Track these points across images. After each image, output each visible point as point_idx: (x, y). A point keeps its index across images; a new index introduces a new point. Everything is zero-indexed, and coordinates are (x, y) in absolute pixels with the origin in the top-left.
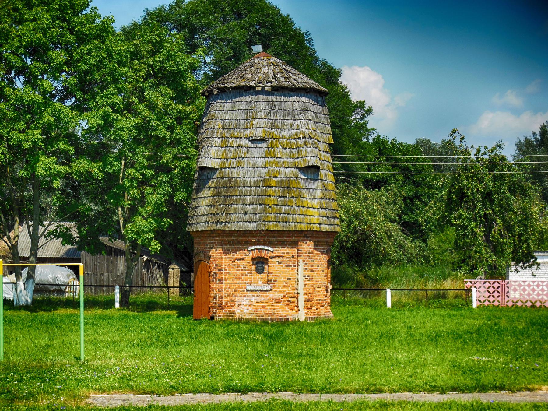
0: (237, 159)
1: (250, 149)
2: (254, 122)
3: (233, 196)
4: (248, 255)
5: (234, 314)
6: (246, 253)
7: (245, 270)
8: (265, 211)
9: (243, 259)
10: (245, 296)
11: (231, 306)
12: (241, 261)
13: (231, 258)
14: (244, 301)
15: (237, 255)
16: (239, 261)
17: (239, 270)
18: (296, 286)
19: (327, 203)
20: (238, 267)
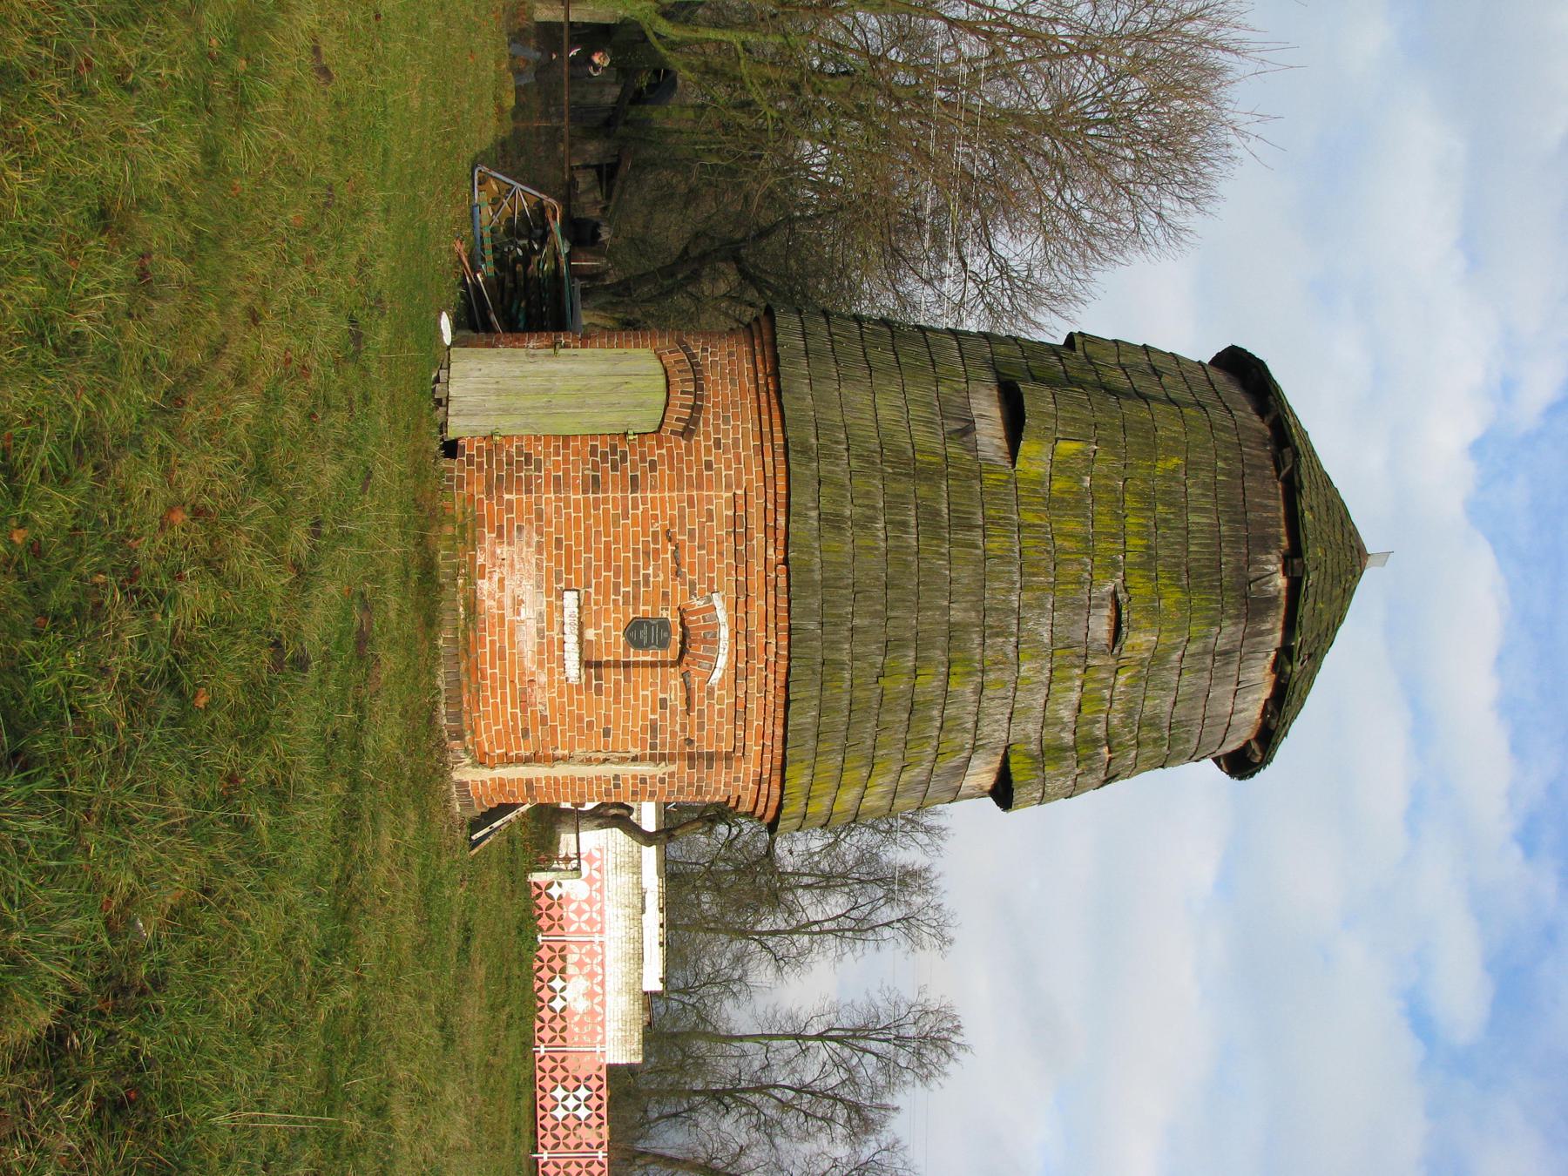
4: (692, 593)
7: (636, 584)
9: (677, 573)
13: (682, 525)
17: (636, 558)
20: (646, 553)
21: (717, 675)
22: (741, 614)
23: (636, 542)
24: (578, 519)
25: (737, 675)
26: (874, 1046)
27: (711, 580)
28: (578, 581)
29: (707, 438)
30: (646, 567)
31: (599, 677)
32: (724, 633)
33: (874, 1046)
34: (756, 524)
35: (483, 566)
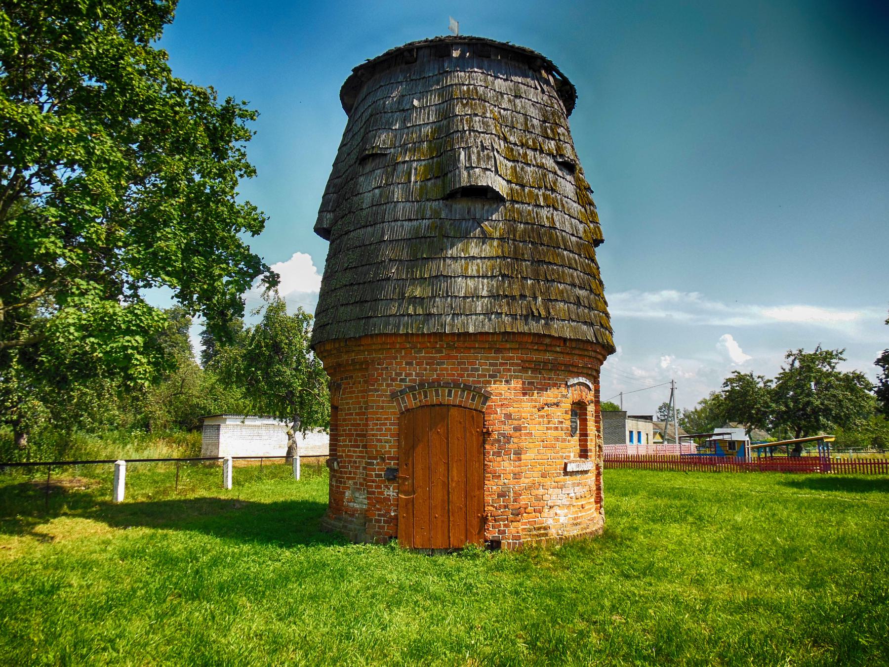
3: (550, 263)
5: (545, 529)
6: (563, 389)
9: (557, 405)
12: (554, 409)
19: (574, 329)
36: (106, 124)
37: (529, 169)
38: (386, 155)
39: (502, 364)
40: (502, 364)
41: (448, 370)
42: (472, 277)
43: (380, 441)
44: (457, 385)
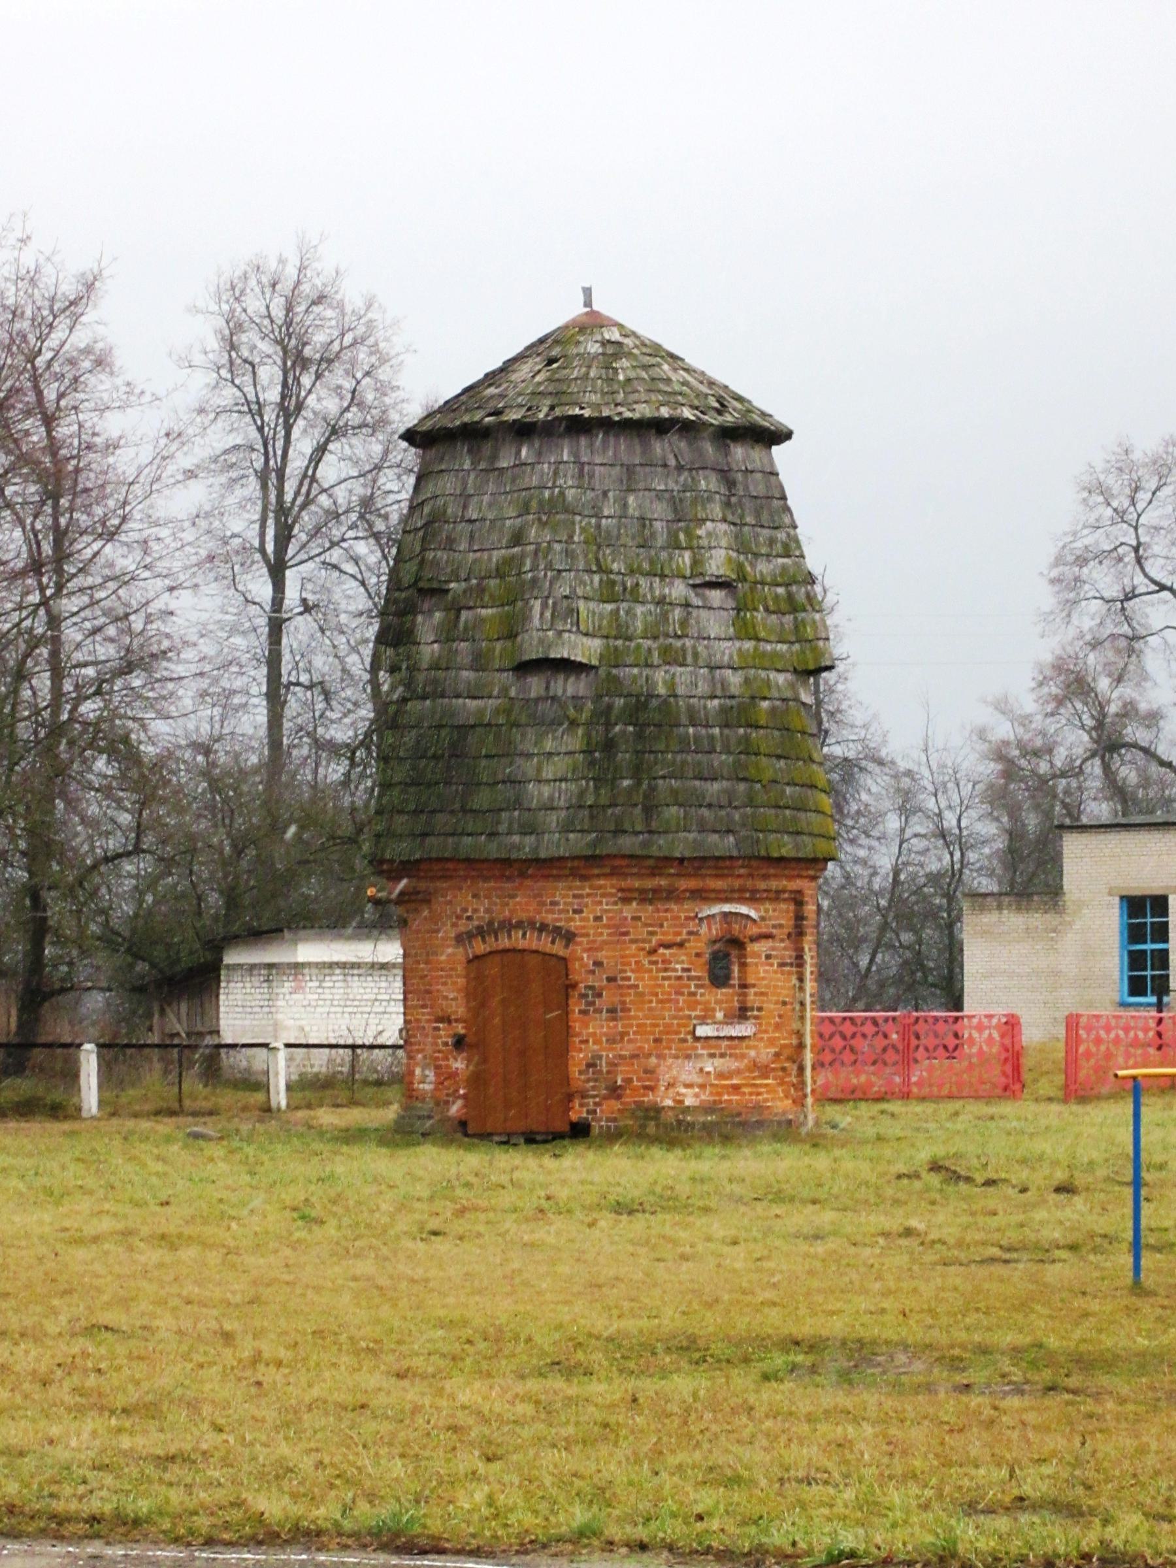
0: (661, 640)
1: (695, 613)
2: (700, 532)
4: (696, 933)
7: (689, 978)
8: (751, 802)
9: (681, 945)
10: (688, 1057)
11: (646, 1088)
13: (644, 941)
14: (687, 1071)
15: (663, 934)
16: (667, 952)
17: (669, 978)
18: (795, 1026)
20: (666, 970)
21: (753, 914)
22: (713, 895)
23: (657, 978)
24: (638, 1026)
25: (753, 898)
26: (296, 464)
27: (687, 918)
28: (685, 1026)
29: (572, 919)
30: (676, 970)
31: (752, 1009)
32: (727, 908)
33: (296, 464)
34: (650, 883)
35: (675, 1101)
36: (112, 752)
37: (639, 610)
38: (448, 591)
39: (589, 895)
40: (589, 895)
41: (520, 903)
42: (548, 781)
43: (446, 998)
44: (532, 923)
